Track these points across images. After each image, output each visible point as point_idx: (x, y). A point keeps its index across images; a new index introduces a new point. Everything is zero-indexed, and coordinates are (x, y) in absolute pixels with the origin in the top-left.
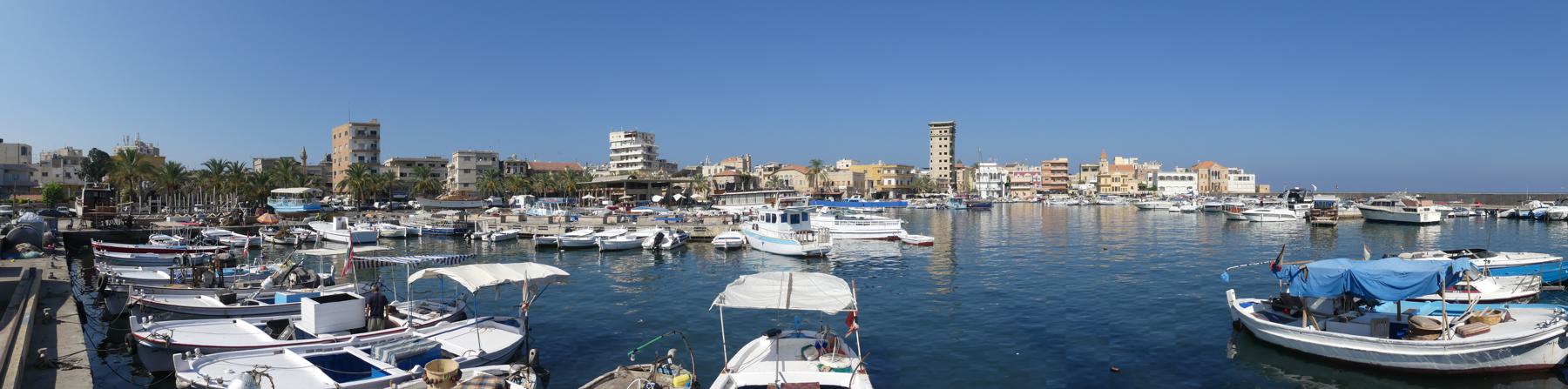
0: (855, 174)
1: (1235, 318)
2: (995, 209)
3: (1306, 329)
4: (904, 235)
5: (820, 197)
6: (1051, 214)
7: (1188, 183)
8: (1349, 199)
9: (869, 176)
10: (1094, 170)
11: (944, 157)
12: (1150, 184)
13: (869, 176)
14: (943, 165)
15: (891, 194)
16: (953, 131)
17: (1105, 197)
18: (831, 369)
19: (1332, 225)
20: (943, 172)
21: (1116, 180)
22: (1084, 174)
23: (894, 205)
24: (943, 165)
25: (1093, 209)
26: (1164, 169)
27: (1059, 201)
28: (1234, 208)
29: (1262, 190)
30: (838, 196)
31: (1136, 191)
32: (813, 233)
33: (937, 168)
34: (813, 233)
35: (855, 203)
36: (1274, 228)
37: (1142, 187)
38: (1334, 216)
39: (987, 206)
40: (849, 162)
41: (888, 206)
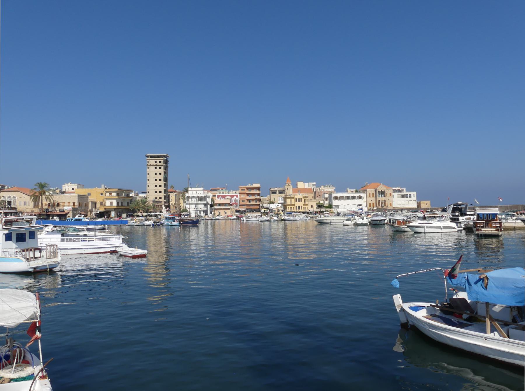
0: (80, 197)
1: (403, 320)
2: (202, 225)
3: (491, 335)
4: (125, 249)
5: (45, 217)
6: (246, 228)
7: (358, 201)
8: (512, 210)
9: (92, 198)
10: (281, 192)
11: (158, 183)
12: (326, 203)
13: (92, 198)
14: (158, 189)
15: (113, 214)
16: (166, 162)
17: (290, 214)
18: (11, 380)
19: (497, 236)
20: (158, 195)
21: (299, 200)
22: (273, 196)
23: (115, 223)
24: (158, 189)
25: (281, 225)
26: (337, 191)
27: (253, 218)
28: (399, 221)
29: (423, 205)
30: (63, 216)
31: (315, 209)
32: (40, 250)
33: (153, 192)
34: (40, 250)
35: (79, 222)
36: (436, 240)
37: (320, 206)
38: (500, 227)
39: (195, 223)
40: (75, 186)
41: (110, 223)
